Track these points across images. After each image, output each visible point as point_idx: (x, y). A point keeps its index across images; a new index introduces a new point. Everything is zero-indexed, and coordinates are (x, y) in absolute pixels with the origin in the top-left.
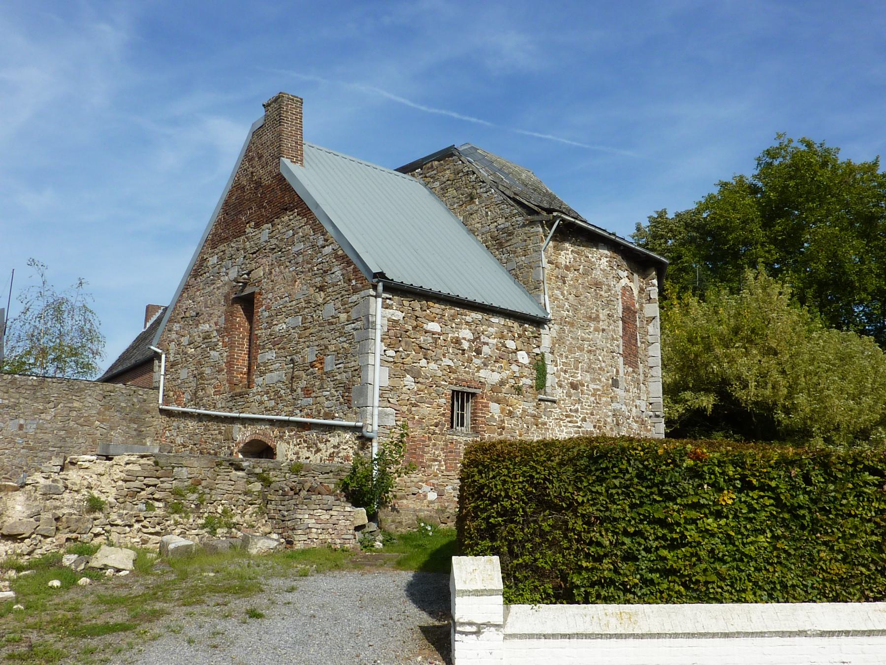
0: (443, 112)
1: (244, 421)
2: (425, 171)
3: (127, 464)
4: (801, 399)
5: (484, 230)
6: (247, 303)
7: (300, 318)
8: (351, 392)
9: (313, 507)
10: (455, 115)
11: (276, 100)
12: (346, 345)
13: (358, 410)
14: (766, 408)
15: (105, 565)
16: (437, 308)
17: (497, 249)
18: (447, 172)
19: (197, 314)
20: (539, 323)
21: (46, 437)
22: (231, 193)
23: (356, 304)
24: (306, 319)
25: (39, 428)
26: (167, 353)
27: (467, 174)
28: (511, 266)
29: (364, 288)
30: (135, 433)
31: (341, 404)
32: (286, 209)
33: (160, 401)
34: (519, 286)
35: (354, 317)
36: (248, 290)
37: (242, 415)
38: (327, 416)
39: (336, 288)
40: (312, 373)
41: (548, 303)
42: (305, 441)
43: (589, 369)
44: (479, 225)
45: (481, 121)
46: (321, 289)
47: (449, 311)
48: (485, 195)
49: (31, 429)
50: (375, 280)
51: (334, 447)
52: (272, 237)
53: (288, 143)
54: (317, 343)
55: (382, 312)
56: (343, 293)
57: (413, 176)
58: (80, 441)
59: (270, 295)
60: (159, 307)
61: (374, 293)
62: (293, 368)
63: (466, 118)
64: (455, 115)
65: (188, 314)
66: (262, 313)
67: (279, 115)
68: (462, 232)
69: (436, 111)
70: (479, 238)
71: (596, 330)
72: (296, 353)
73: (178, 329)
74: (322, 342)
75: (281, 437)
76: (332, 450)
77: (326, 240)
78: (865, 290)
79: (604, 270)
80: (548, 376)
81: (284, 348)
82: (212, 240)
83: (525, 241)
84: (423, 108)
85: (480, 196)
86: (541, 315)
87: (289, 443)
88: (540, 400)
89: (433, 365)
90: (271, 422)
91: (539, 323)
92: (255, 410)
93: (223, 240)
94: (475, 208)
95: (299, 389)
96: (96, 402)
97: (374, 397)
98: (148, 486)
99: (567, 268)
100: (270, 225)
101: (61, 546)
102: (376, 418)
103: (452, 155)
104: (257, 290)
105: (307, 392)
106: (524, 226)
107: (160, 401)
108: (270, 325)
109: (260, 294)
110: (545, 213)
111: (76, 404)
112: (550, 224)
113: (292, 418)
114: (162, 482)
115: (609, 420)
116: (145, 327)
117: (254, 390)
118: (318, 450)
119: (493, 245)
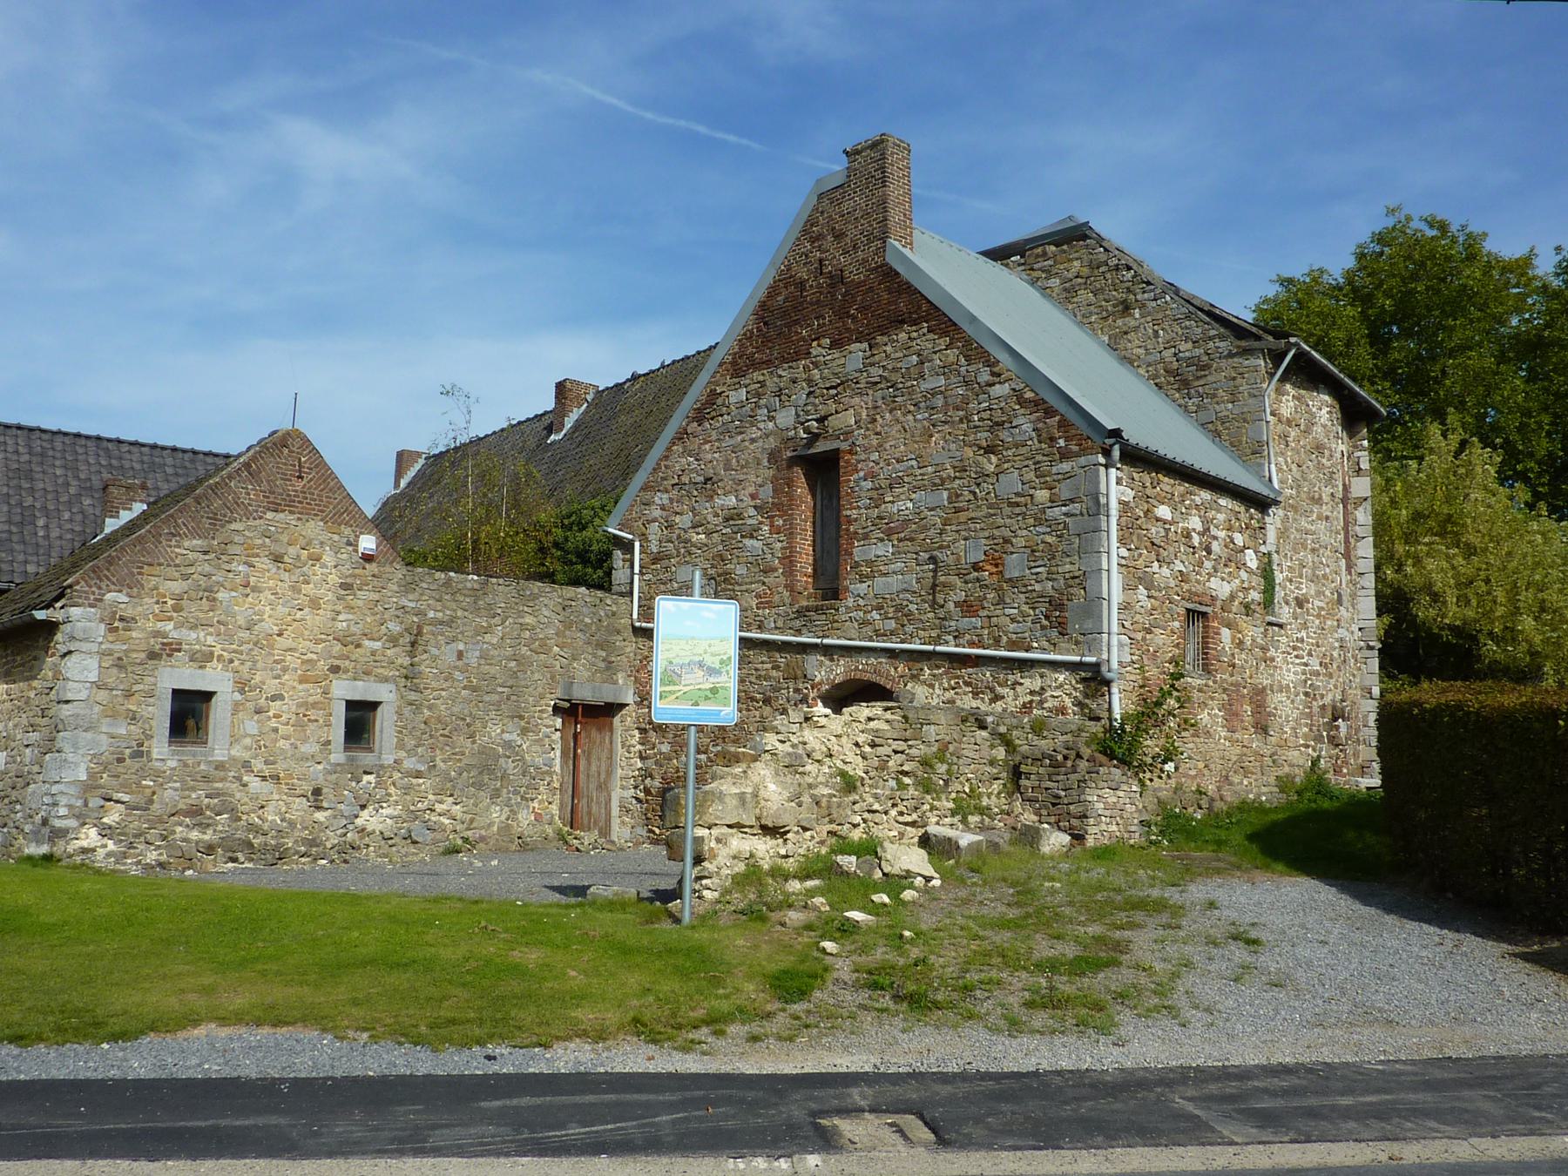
0: (683, 123)
1: (828, 651)
2: (1031, 260)
3: (870, 719)
4: (1527, 623)
5: (1151, 358)
6: (822, 469)
7: (945, 494)
8: (1066, 610)
9: (1102, 784)
10: (702, 129)
11: (874, 145)
12: (1049, 539)
13: (1081, 638)
14: (1466, 636)
15: (908, 871)
16: (1167, 482)
17: (1178, 390)
18: (1075, 263)
19: (707, 480)
20: (1260, 503)
21: (494, 670)
22: (773, 292)
23: (1068, 476)
24: (958, 496)
25: (484, 656)
26: (644, 537)
27: (1117, 268)
28: (1203, 417)
29: (1083, 452)
30: (603, 665)
31: (1043, 628)
32: (903, 322)
33: (635, 616)
34: (1223, 448)
35: (1065, 495)
36: (821, 447)
37: (826, 641)
38: (1013, 646)
39: (1023, 450)
40: (978, 580)
41: (1277, 474)
42: (967, 684)
43: (1314, 579)
44: (1142, 351)
45: (745, 142)
46: (989, 450)
47: (1181, 488)
48: (1154, 304)
49: (472, 658)
50: (1109, 441)
51: (1032, 693)
52: (872, 365)
53: (895, 216)
54: (986, 534)
55: (1116, 487)
56: (1040, 458)
57: (1007, 265)
58: (536, 676)
59: (875, 456)
60: (419, 454)
61: (1102, 460)
62: (935, 571)
63: (720, 135)
64: (702, 129)
65: (685, 479)
66: (857, 483)
67: (883, 169)
68: (1108, 362)
69: (671, 121)
70: (1142, 371)
71: (1319, 518)
72: (941, 547)
73: (666, 502)
74: (996, 532)
75: (914, 677)
76: (1029, 698)
77: (993, 374)
78: (1531, 455)
79: (1324, 426)
80: (1277, 588)
81: (912, 540)
82: (734, 363)
83: (1234, 379)
84: (649, 115)
85: (1144, 305)
86: (1265, 492)
87: (932, 686)
88: (1270, 624)
89: (1165, 571)
90: (892, 654)
91: (1260, 503)
92: (854, 633)
93: (755, 365)
94: (1133, 323)
95: (951, 605)
96: (554, 616)
97: (1112, 619)
98: (896, 752)
99: (1289, 423)
100: (865, 345)
101: (822, 843)
102: (1115, 650)
103: (1085, 237)
104: (845, 446)
105: (967, 608)
106: (1231, 355)
107: (635, 616)
108: (878, 502)
109: (850, 452)
110: (1270, 338)
111: (529, 620)
112: (1277, 358)
113: (939, 648)
114: (910, 747)
115: (1335, 654)
116: (397, 484)
117: (850, 602)
118: (997, 698)
119: (1169, 383)
